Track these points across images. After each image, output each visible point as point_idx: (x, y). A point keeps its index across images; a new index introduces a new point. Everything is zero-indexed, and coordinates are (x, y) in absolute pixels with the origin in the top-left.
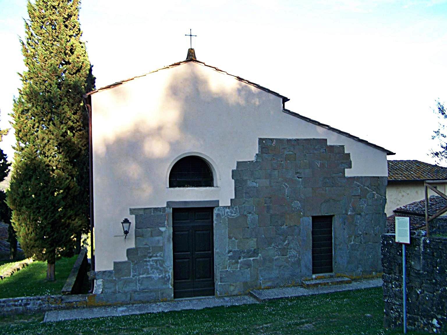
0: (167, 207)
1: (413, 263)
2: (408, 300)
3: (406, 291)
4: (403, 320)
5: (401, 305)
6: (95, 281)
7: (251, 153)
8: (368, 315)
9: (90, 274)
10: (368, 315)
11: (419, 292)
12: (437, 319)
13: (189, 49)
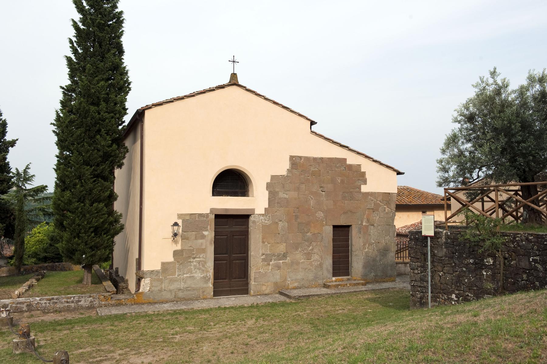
1: (436, 252)
7: (282, 168)
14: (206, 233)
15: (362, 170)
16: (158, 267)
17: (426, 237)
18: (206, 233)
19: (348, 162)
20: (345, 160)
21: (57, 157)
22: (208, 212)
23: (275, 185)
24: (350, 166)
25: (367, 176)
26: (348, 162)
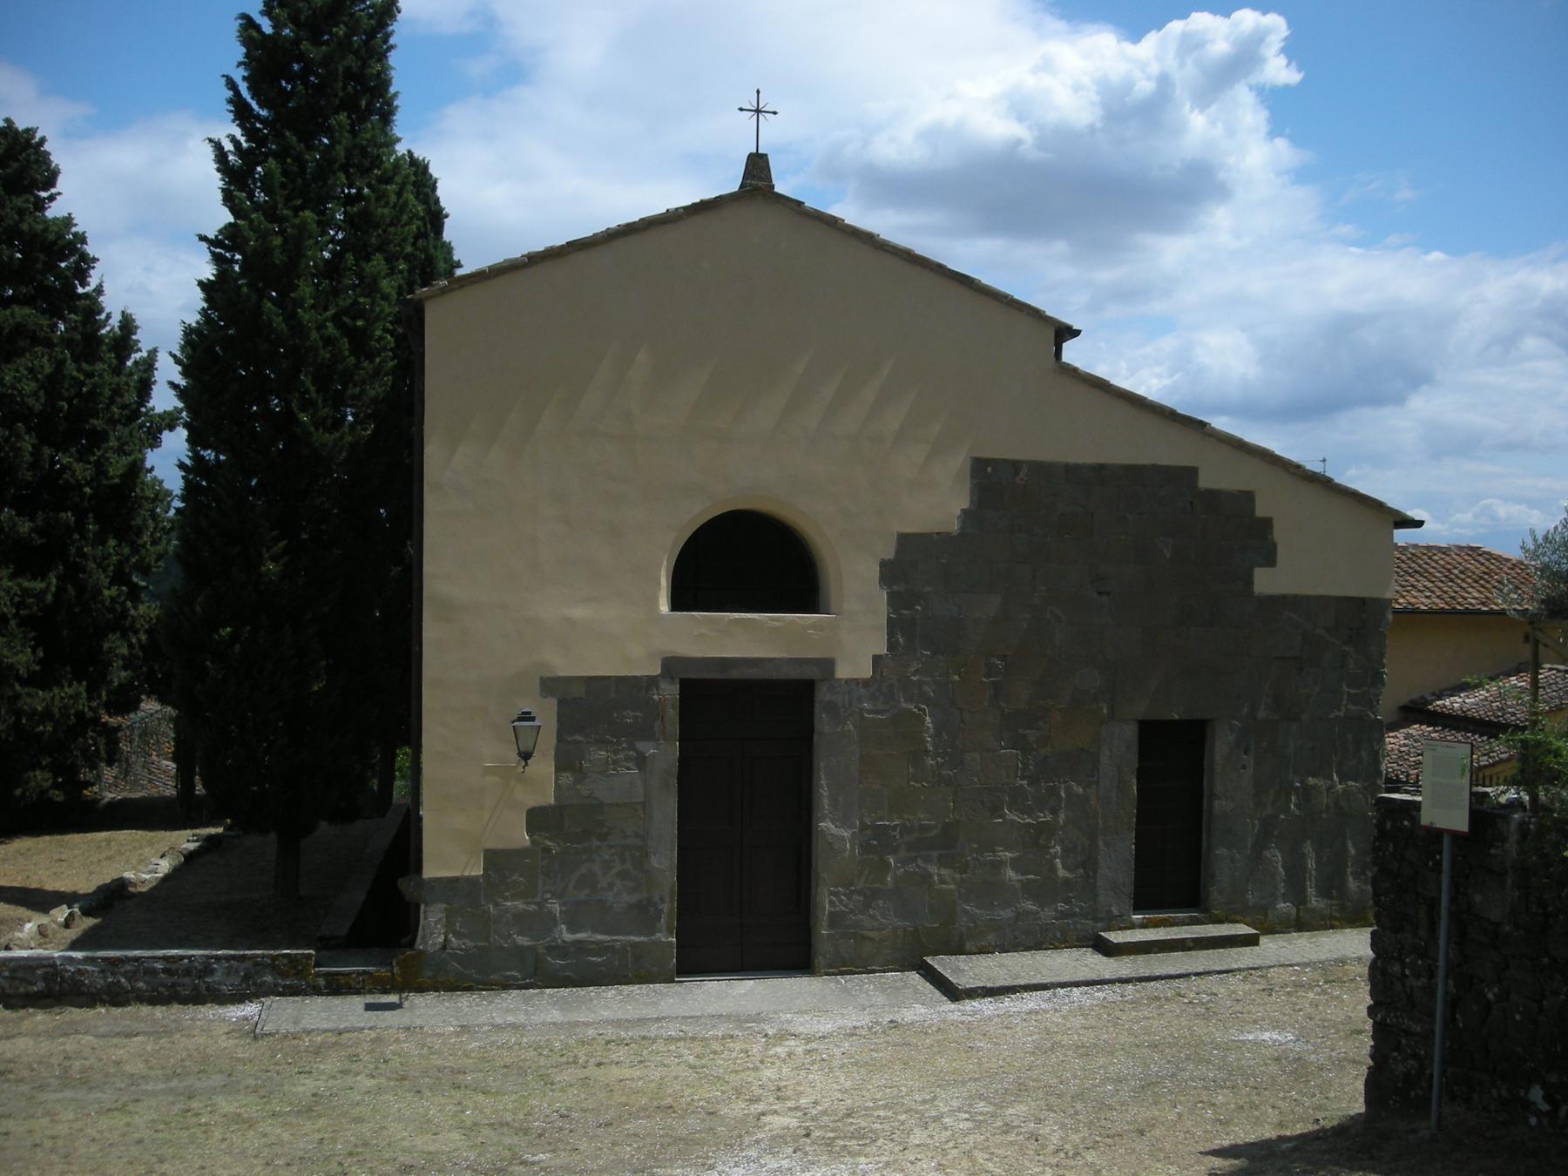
0: (662, 675)
1: (1478, 898)
2: (1454, 1020)
3: (1446, 993)
4: (1431, 1086)
5: (1428, 1036)
6: (422, 907)
7: (942, 505)
8: (65, 632)
9: (406, 886)
10: (65, 632)
11: (1490, 996)
12: (1544, 1085)
13: (751, 156)
14: (649, 749)
15: (1260, 512)
16: (476, 869)
17: (1436, 834)
18: (649, 749)
19: (1205, 481)
20: (1192, 473)
21: (182, 466)
22: (655, 670)
23: (912, 567)
24: (1213, 496)
25: (1279, 534)
26: (1205, 481)
